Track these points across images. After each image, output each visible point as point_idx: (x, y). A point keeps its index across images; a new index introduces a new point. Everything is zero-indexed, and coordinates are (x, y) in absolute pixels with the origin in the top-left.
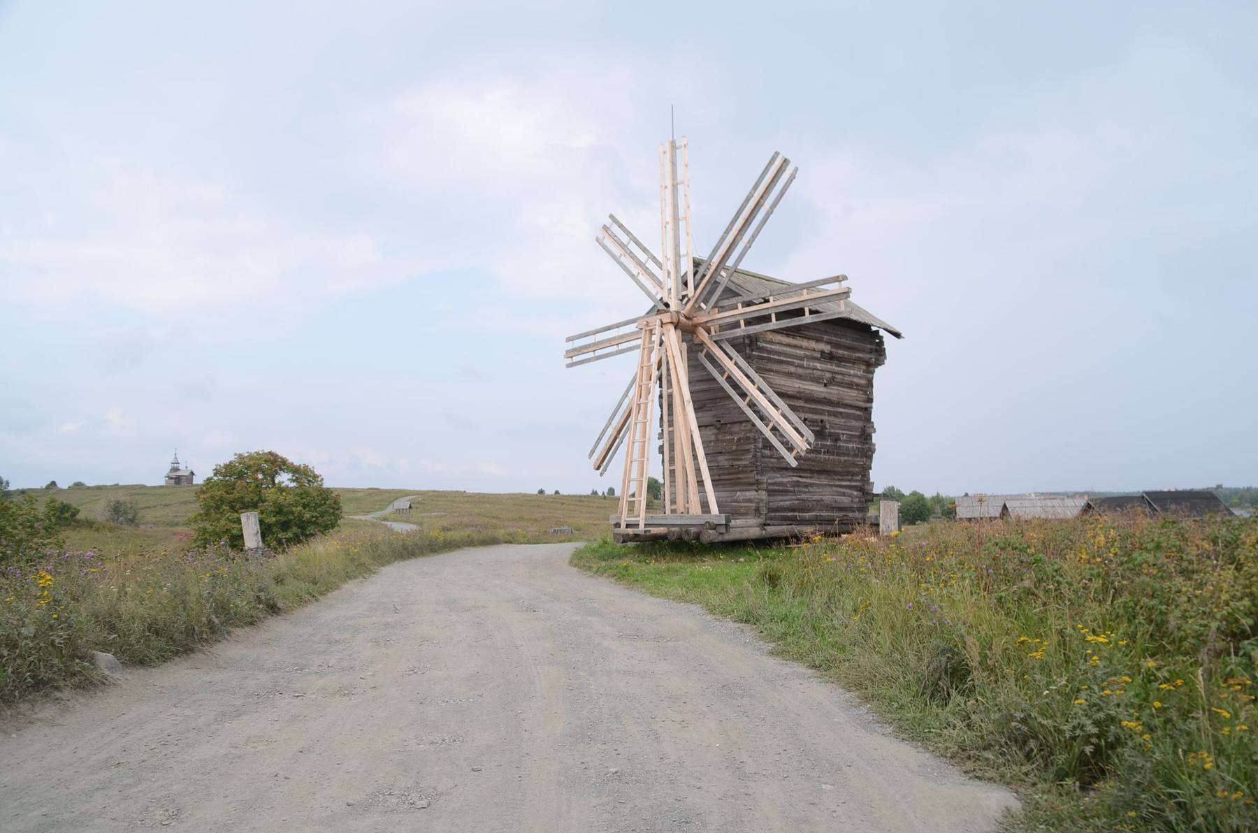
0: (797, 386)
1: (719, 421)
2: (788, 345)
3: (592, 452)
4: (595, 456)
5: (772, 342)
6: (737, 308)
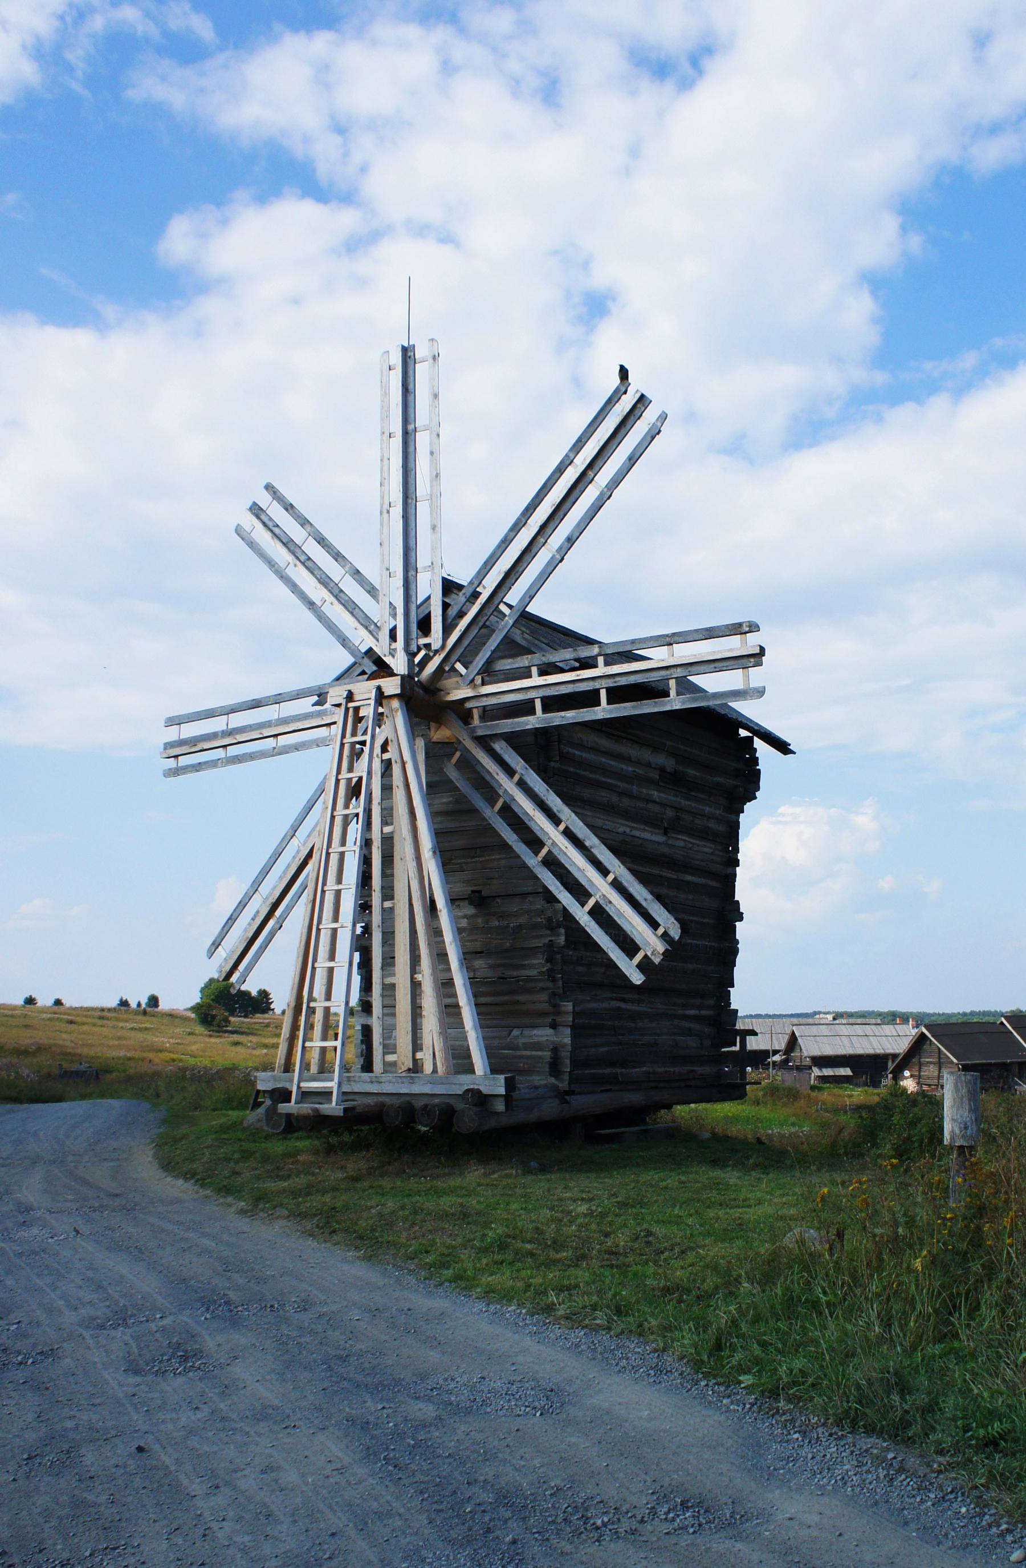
0: (621, 829)
1: (480, 892)
2: (608, 754)
3: (216, 944)
4: (221, 953)
5: (581, 746)
6: (529, 676)
